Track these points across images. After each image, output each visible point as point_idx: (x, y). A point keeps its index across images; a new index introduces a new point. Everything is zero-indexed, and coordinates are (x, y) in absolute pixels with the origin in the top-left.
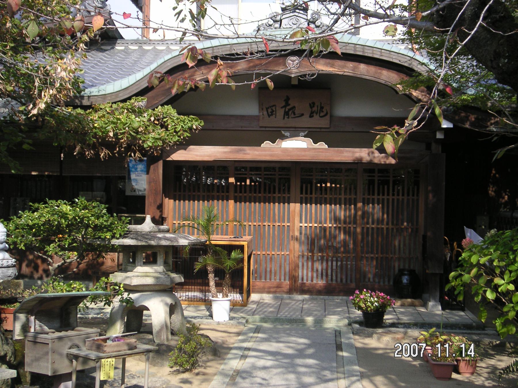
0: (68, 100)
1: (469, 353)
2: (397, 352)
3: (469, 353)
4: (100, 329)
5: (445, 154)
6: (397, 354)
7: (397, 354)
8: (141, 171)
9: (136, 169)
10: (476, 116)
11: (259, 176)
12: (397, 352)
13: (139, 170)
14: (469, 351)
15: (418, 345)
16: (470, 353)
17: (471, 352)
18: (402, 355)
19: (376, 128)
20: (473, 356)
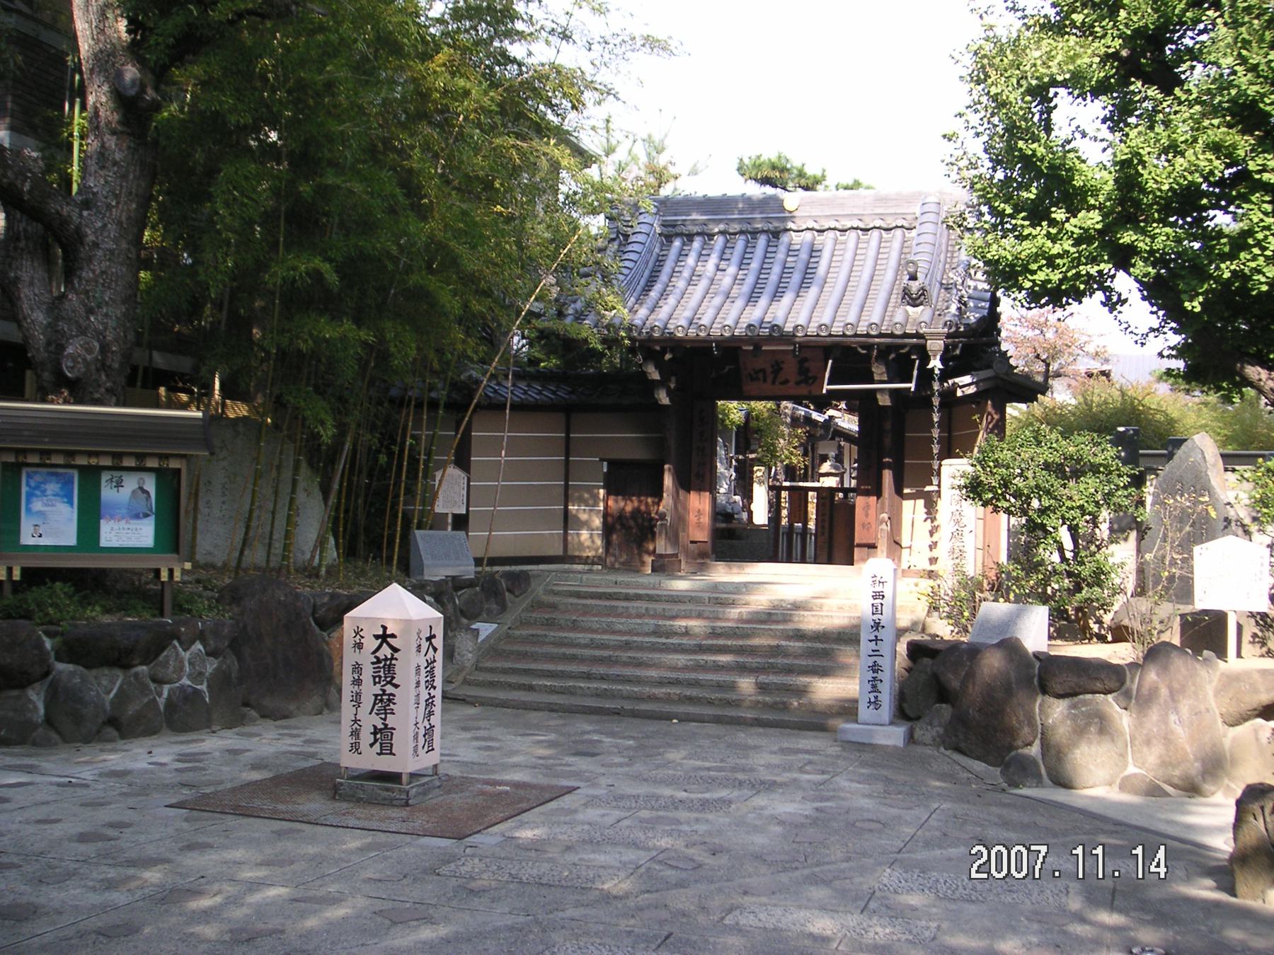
0: (185, 255)
1: (1153, 869)
2: (975, 866)
3: (1153, 869)
4: (250, 904)
5: (101, 545)
6: (977, 872)
7: (977, 872)
8: (54, 495)
9: (44, 491)
10: (913, 390)
11: (89, 794)
12: (975, 866)
13: (49, 492)
14: (1154, 864)
15: (1029, 850)
16: (1157, 870)
17: (1158, 865)
18: (989, 873)
19: (79, 760)
20: (1162, 876)
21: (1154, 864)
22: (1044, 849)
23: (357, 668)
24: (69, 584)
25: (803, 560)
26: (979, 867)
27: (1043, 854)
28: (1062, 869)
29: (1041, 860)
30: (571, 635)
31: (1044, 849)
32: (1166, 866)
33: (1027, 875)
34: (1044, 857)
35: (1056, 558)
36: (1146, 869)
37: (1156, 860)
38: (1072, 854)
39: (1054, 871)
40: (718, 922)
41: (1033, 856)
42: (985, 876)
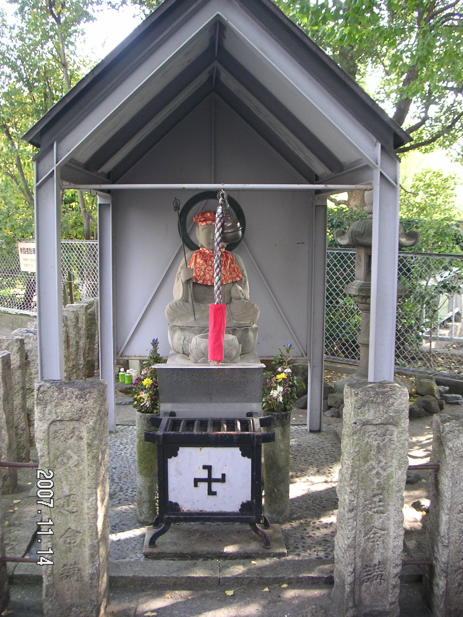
3: (42, 558)
6: (40, 473)
7: (40, 473)
15: (51, 498)
16: (41, 560)
17: (43, 561)
18: (40, 479)
21: (44, 559)
22: (51, 505)
23: (333, 359)
24: (360, 66)
25: (370, 284)
26: (43, 474)
27: (49, 505)
28: (42, 543)
29: (46, 504)
30: (329, 365)
31: (51, 505)
32: (43, 565)
33: (39, 497)
34: (47, 506)
35: (198, 260)
36: (42, 555)
37: (46, 560)
38: (49, 519)
39: (41, 510)
40: (18, 159)
41: (48, 500)
42: (38, 477)
